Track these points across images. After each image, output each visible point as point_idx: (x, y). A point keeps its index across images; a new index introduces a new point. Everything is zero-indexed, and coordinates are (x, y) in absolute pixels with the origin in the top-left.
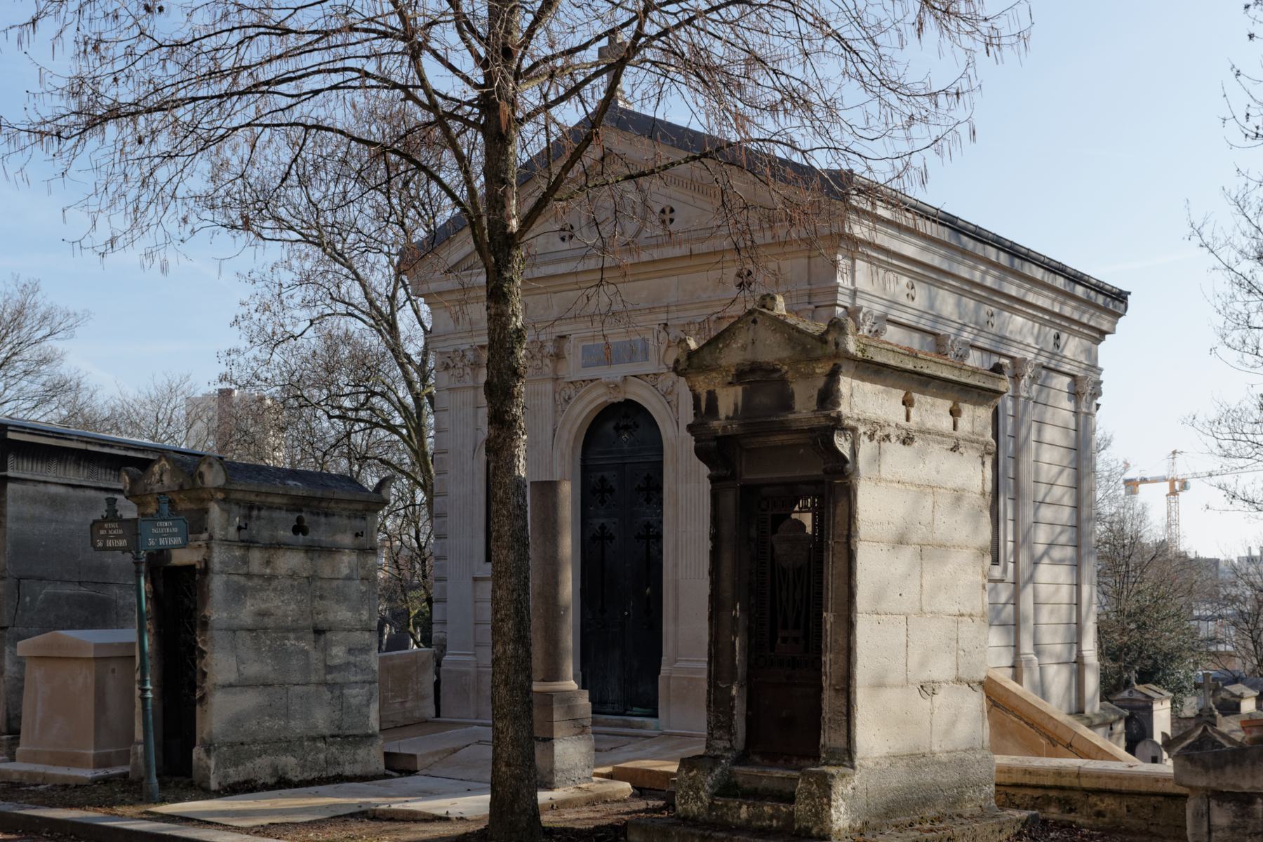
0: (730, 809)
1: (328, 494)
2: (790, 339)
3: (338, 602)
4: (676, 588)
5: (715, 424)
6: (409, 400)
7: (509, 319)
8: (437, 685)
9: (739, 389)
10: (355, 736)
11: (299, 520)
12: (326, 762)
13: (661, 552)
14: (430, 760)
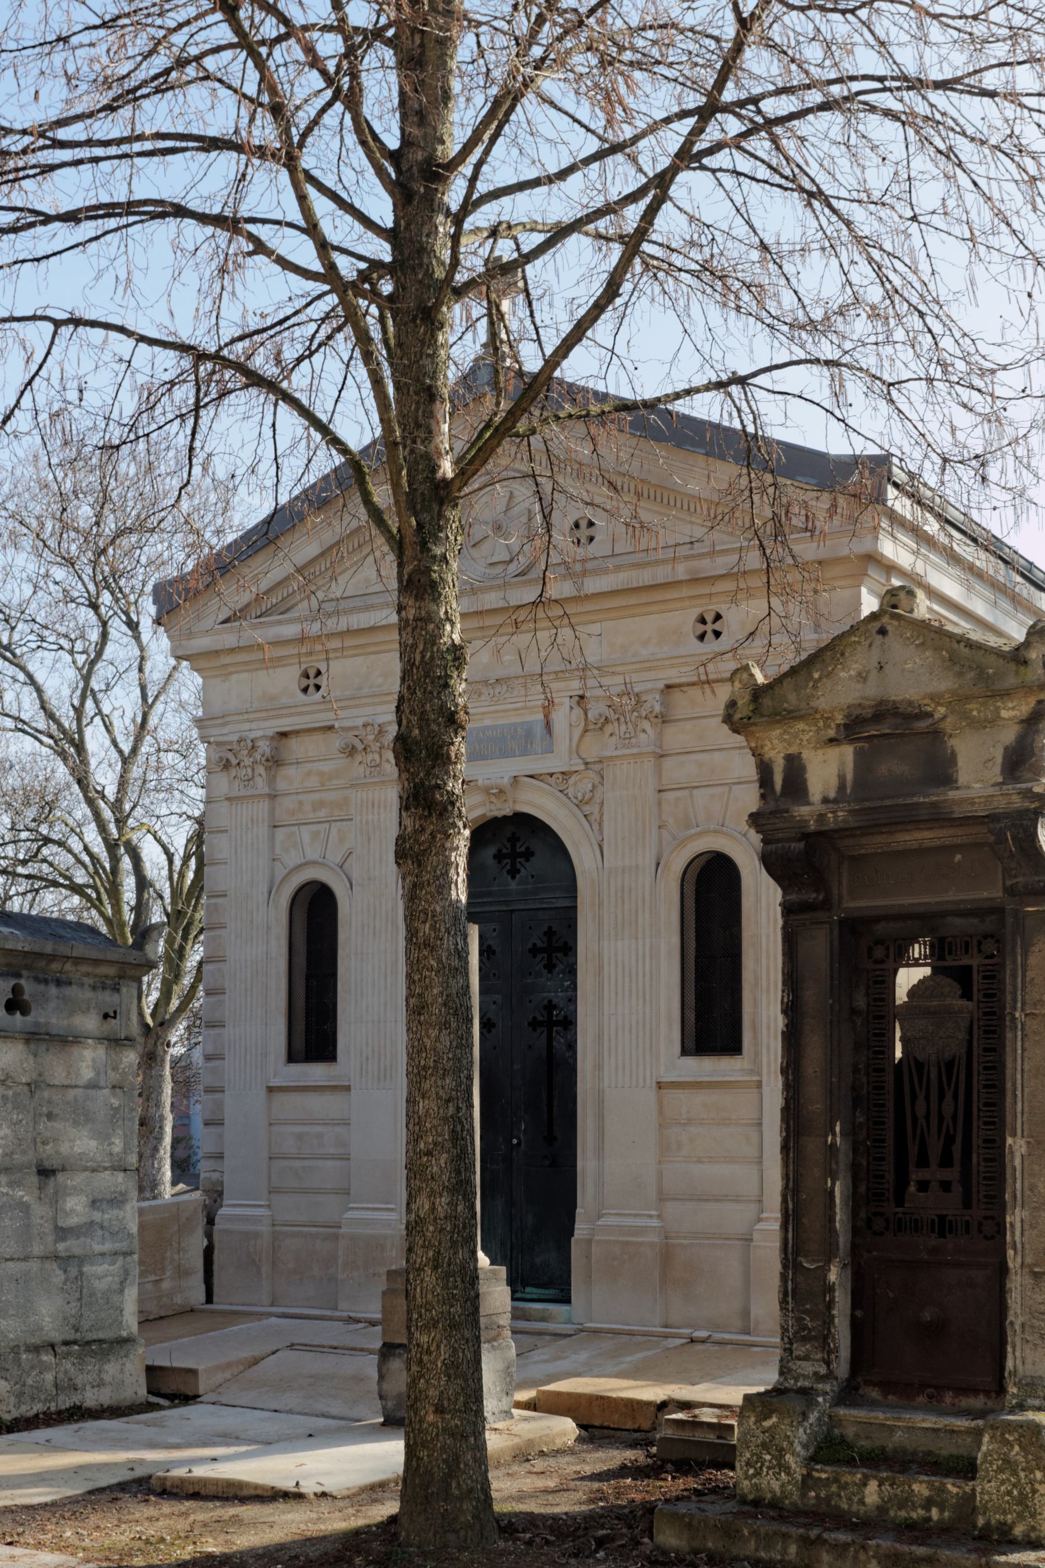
0: (844, 1487)
1: (63, 949)
2: (953, 659)
3: (76, 1124)
4: (600, 1101)
5: (804, 810)
6: (99, 848)
7: (440, 626)
8: (208, 1253)
9: (848, 751)
10: (100, 1341)
11: (17, 990)
12: (56, 1386)
13: (572, 1046)
14: (219, 1377)
